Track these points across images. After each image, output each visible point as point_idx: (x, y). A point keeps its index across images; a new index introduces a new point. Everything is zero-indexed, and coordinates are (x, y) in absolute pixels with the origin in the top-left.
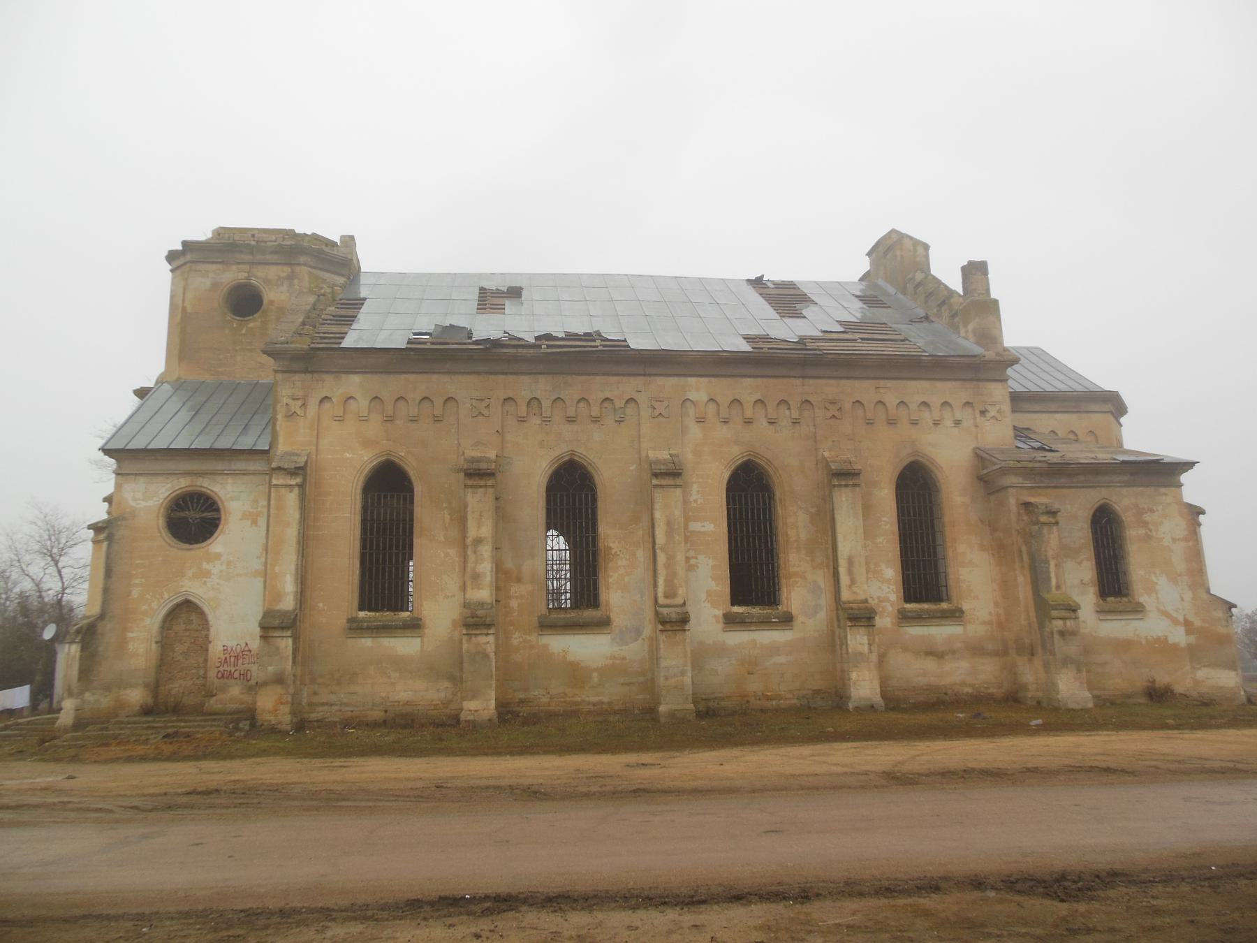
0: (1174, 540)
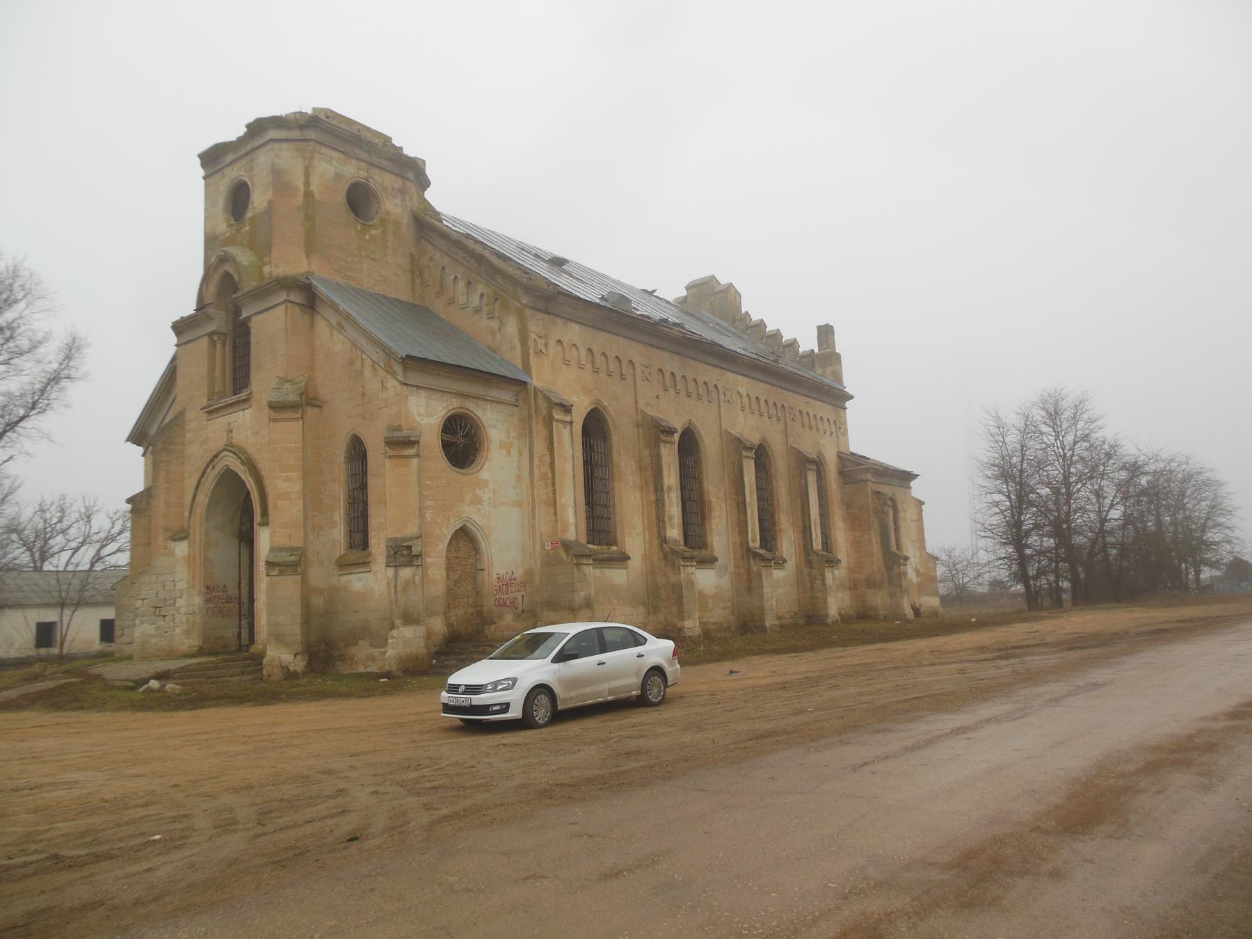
0: (912, 521)
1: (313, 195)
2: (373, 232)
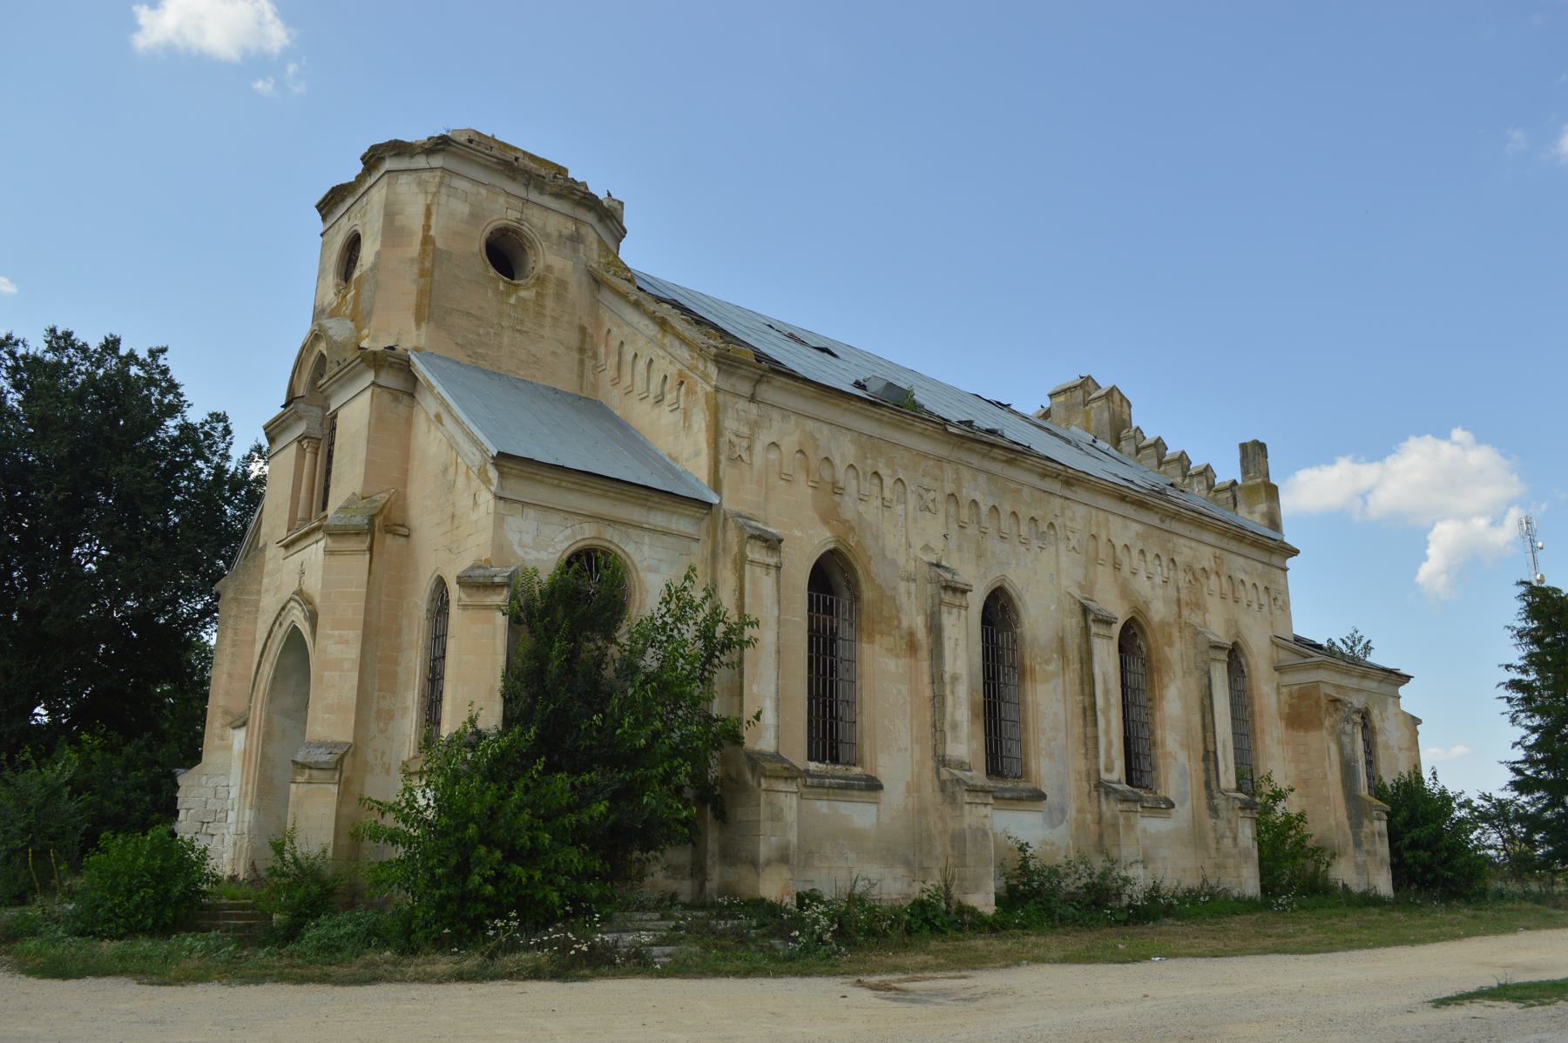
1: (434, 243)
2: (523, 294)
